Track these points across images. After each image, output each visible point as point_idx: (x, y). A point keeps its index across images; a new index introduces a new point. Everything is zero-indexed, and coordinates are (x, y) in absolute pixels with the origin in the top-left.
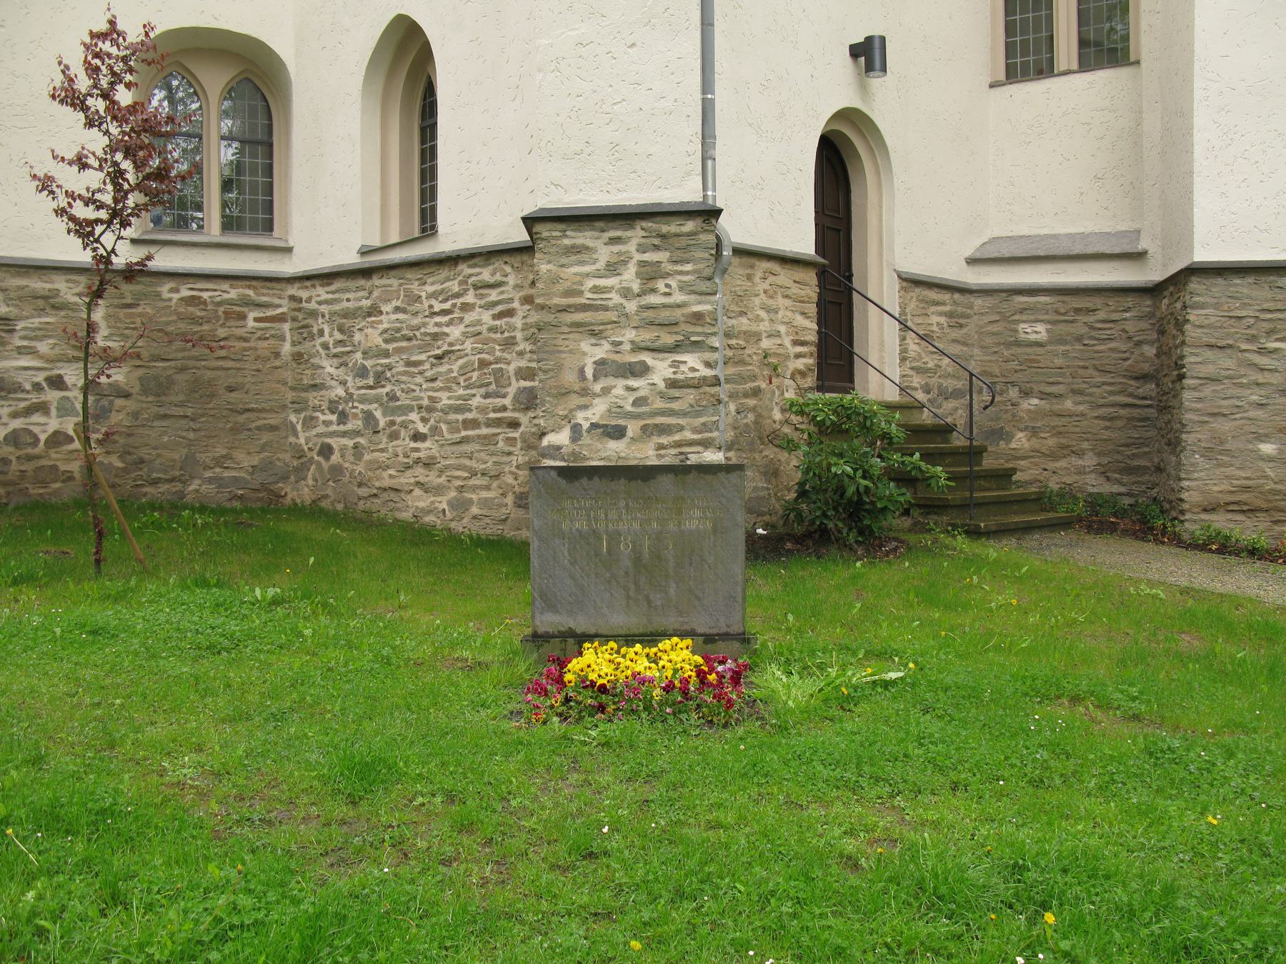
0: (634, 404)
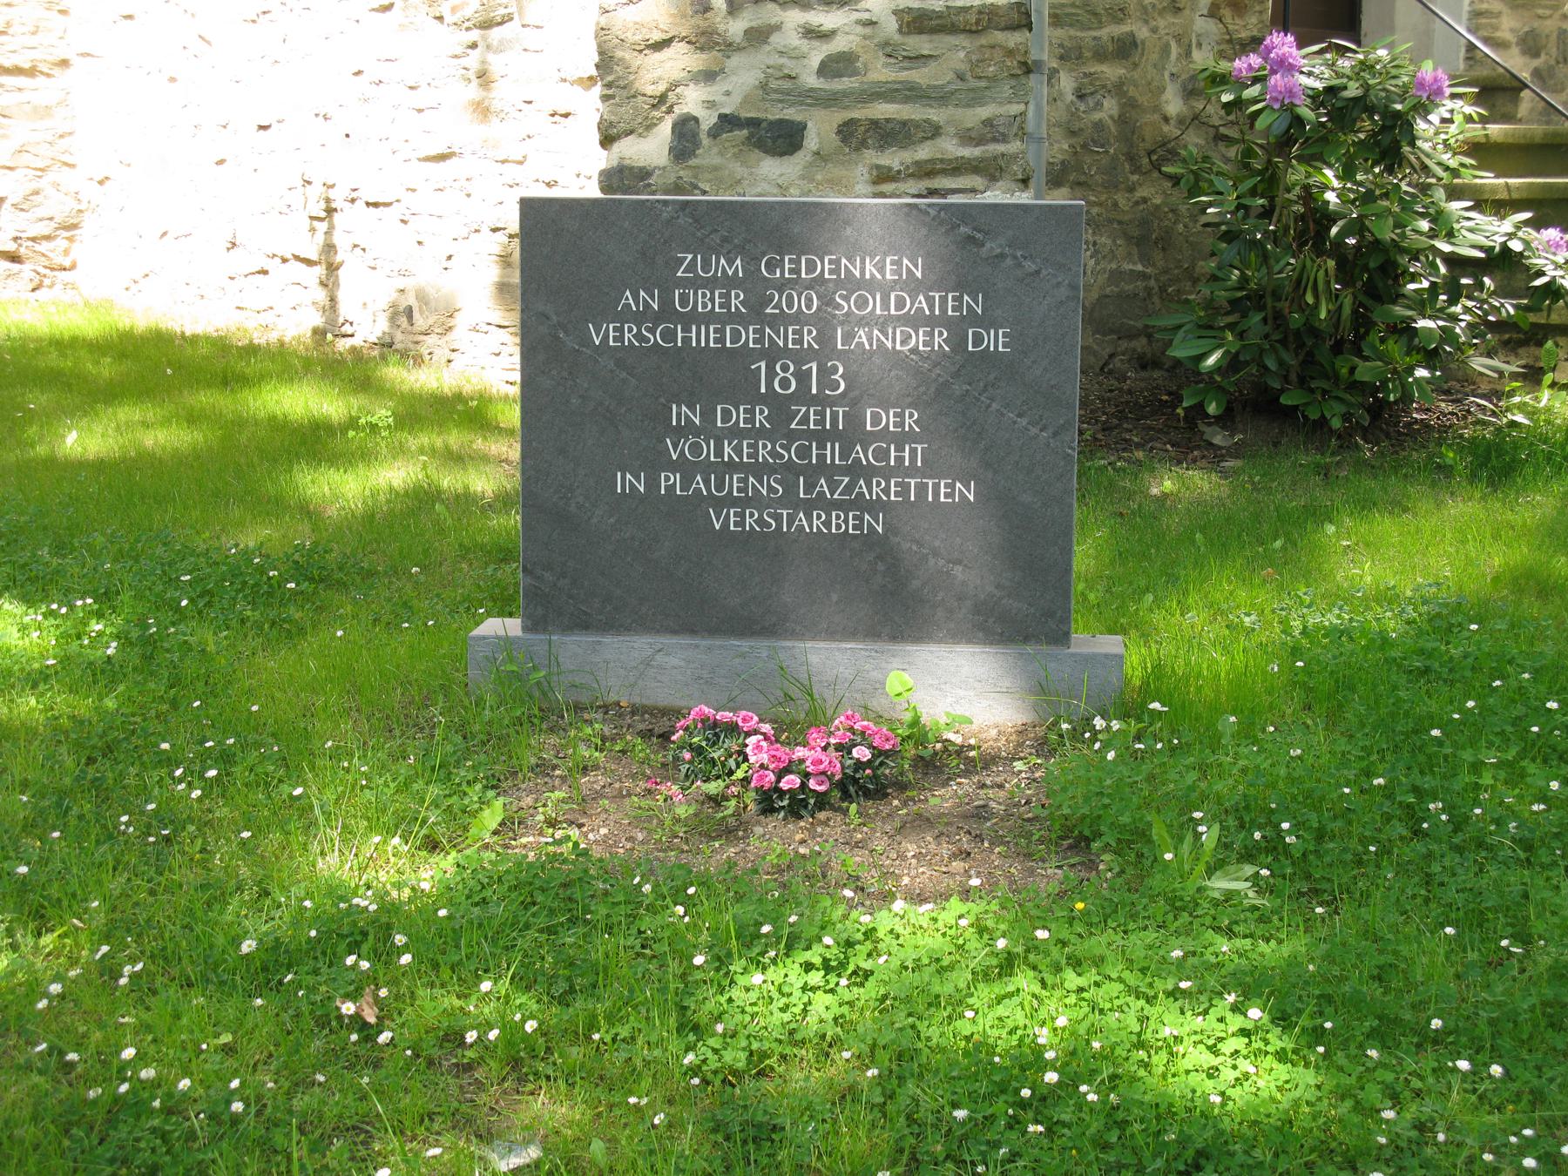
0: (825, 69)
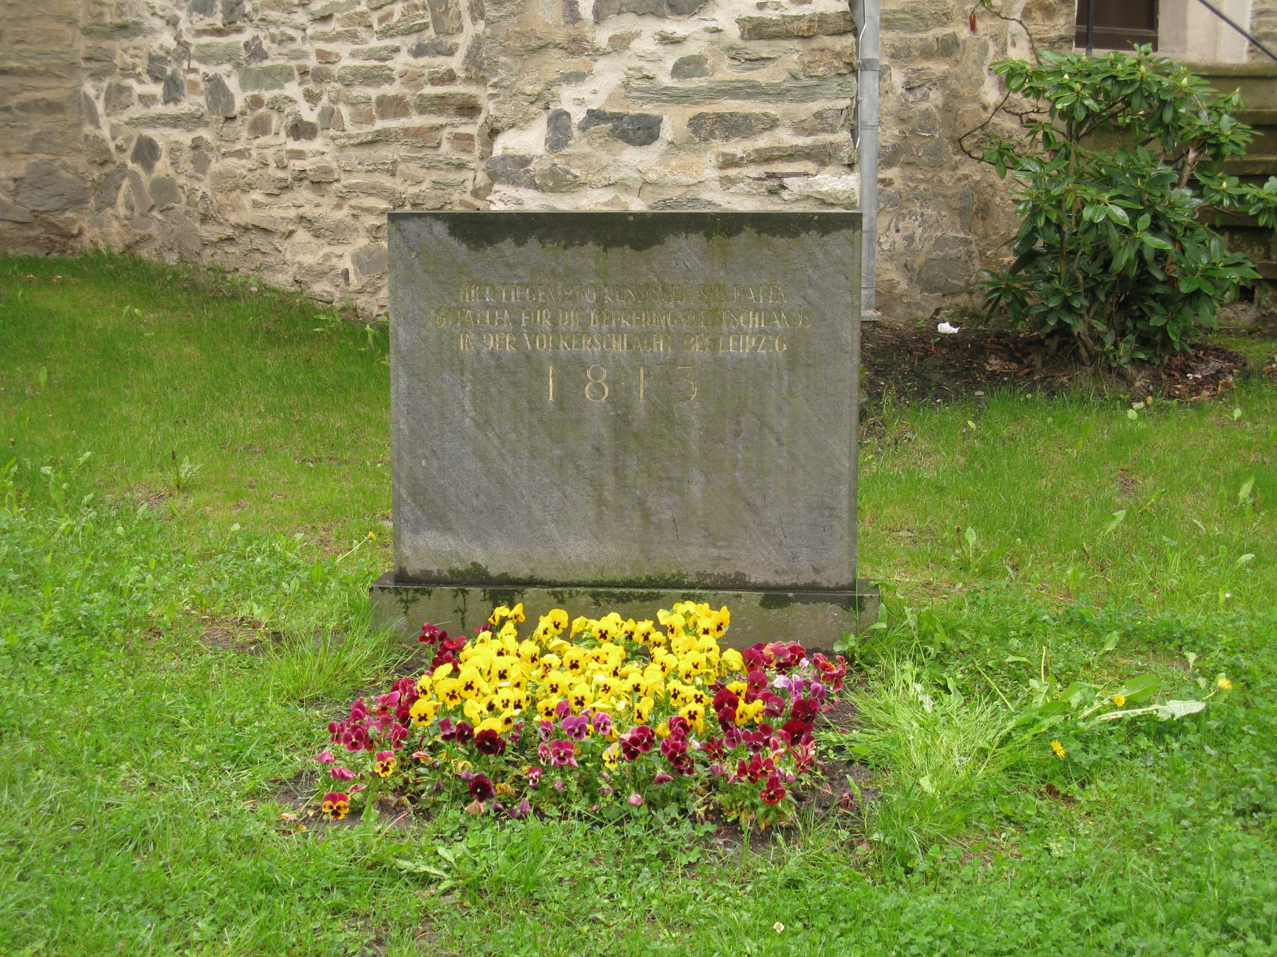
0: (677, 71)
